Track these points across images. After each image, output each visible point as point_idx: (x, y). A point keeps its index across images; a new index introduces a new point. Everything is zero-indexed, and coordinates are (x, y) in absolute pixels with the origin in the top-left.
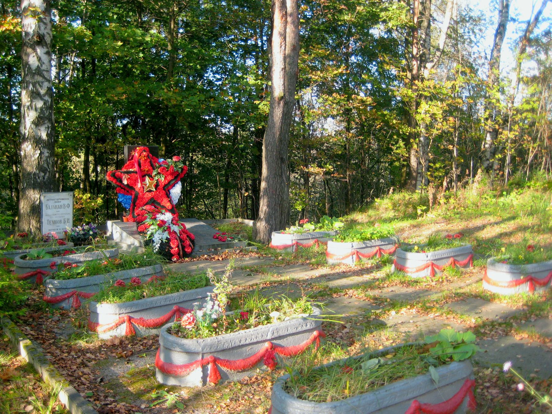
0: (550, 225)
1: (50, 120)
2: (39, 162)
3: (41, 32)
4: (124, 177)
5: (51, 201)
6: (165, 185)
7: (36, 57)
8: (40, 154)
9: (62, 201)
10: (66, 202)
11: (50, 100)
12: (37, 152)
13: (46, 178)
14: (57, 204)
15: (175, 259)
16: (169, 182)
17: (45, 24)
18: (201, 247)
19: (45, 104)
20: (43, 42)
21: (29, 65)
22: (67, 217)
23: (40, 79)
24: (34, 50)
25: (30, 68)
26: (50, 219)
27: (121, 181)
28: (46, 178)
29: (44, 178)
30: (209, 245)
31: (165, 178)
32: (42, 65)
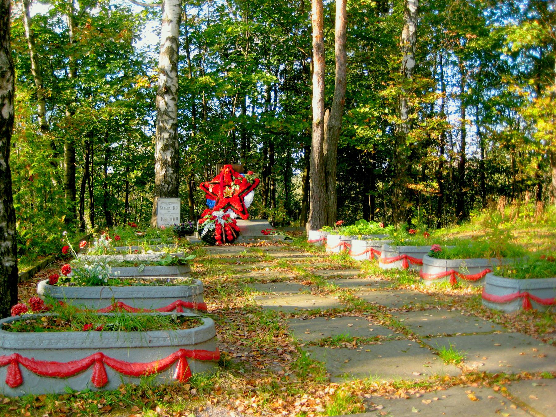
1: (174, 147)
3: (168, 85)
8: (166, 171)
11: (174, 133)
13: (169, 188)
14: (168, 206)
15: (218, 243)
16: (243, 192)
17: (171, 78)
18: (244, 237)
19: (169, 135)
20: (169, 92)
22: (175, 216)
23: (166, 118)
24: (163, 97)
25: (160, 111)
26: (163, 217)
28: (169, 188)
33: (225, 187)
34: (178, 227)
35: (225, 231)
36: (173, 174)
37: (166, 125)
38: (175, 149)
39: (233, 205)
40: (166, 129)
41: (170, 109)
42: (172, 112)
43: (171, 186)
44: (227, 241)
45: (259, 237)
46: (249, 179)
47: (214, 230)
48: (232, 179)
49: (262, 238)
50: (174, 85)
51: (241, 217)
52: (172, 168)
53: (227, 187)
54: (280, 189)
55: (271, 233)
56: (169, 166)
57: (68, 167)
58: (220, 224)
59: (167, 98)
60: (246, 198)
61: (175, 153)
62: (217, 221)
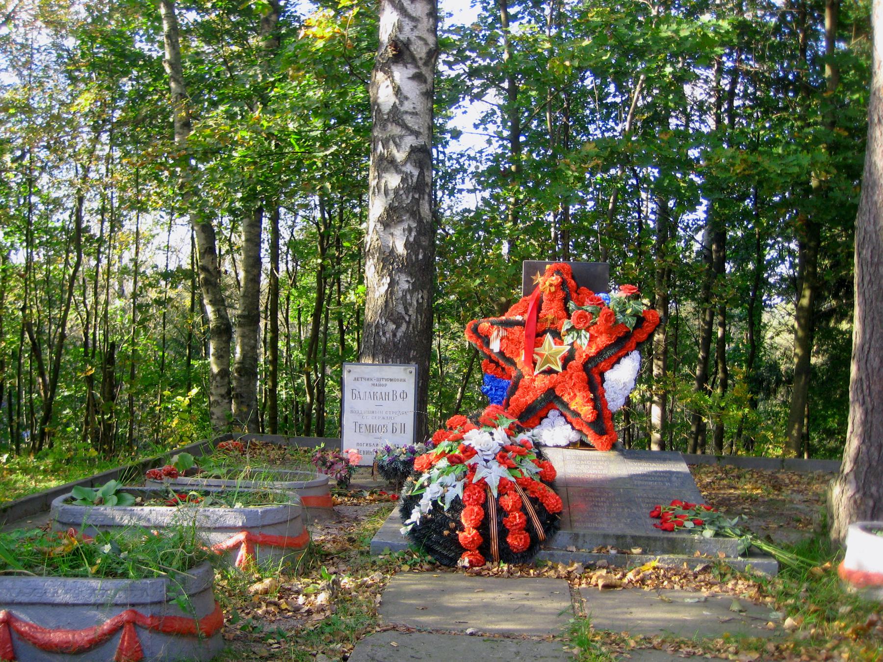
0: (266, 2)
2: (386, 302)
4: (495, 333)
5: (364, 382)
6: (590, 359)
7: (391, 88)
9: (389, 383)
10: (399, 387)
11: (416, 173)
12: (384, 280)
13: (399, 334)
14: (377, 389)
16: (600, 353)
20: (406, 56)
21: (378, 105)
22: (399, 419)
23: (396, 130)
24: (389, 74)
26: (360, 421)
27: (487, 342)
28: (399, 334)
29: (394, 335)
30: (606, 536)
31: (592, 339)
32: (401, 103)
33: (540, 334)
34: (395, 459)
35: (500, 510)
36: (411, 291)
37: (395, 151)
38: (420, 221)
39: (566, 398)
40: (392, 162)
41: (407, 106)
42: (414, 114)
43: (404, 327)
44: (506, 555)
45: (636, 541)
46: (623, 312)
47: (457, 505)
48: (567, 310)
49: (649, 546)
50: (420, 38)
51: (590, 440)
52: (410, 274)
53: (548, 337)
54: (739, 334)
55: (690, 525)
56: (399, 270)
57: (246, 278)
58: (483, 485)
59: (400, 74)
60: (609, 375)
61: (419, 233)
62: (473, 469)
